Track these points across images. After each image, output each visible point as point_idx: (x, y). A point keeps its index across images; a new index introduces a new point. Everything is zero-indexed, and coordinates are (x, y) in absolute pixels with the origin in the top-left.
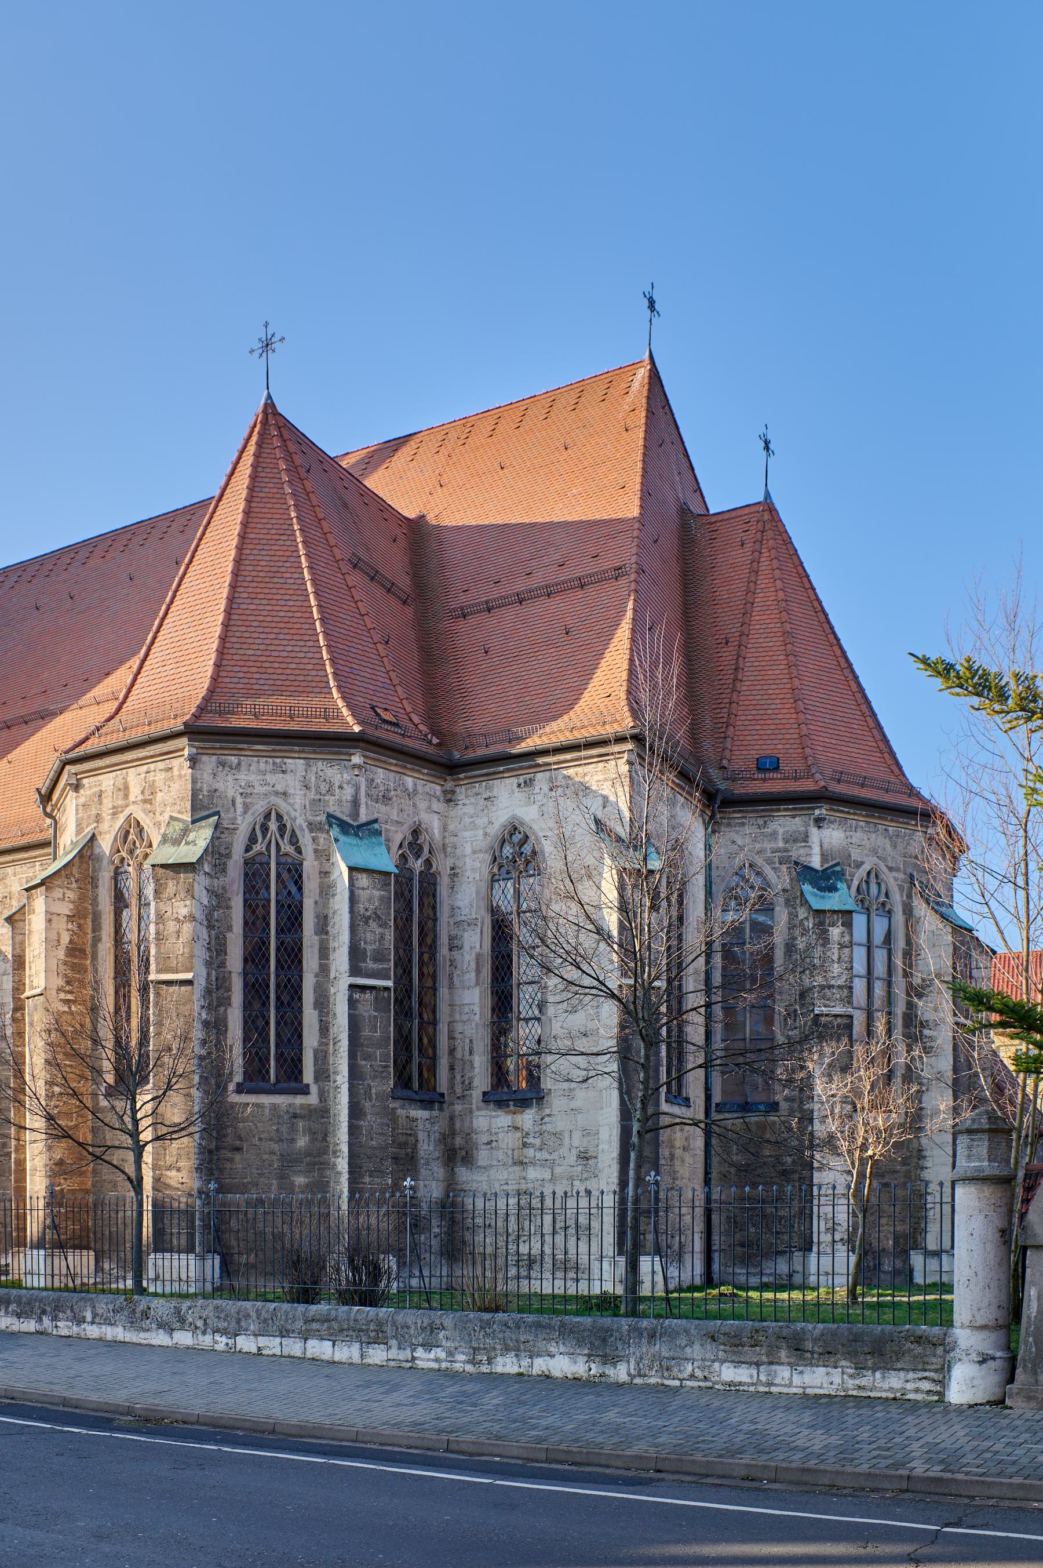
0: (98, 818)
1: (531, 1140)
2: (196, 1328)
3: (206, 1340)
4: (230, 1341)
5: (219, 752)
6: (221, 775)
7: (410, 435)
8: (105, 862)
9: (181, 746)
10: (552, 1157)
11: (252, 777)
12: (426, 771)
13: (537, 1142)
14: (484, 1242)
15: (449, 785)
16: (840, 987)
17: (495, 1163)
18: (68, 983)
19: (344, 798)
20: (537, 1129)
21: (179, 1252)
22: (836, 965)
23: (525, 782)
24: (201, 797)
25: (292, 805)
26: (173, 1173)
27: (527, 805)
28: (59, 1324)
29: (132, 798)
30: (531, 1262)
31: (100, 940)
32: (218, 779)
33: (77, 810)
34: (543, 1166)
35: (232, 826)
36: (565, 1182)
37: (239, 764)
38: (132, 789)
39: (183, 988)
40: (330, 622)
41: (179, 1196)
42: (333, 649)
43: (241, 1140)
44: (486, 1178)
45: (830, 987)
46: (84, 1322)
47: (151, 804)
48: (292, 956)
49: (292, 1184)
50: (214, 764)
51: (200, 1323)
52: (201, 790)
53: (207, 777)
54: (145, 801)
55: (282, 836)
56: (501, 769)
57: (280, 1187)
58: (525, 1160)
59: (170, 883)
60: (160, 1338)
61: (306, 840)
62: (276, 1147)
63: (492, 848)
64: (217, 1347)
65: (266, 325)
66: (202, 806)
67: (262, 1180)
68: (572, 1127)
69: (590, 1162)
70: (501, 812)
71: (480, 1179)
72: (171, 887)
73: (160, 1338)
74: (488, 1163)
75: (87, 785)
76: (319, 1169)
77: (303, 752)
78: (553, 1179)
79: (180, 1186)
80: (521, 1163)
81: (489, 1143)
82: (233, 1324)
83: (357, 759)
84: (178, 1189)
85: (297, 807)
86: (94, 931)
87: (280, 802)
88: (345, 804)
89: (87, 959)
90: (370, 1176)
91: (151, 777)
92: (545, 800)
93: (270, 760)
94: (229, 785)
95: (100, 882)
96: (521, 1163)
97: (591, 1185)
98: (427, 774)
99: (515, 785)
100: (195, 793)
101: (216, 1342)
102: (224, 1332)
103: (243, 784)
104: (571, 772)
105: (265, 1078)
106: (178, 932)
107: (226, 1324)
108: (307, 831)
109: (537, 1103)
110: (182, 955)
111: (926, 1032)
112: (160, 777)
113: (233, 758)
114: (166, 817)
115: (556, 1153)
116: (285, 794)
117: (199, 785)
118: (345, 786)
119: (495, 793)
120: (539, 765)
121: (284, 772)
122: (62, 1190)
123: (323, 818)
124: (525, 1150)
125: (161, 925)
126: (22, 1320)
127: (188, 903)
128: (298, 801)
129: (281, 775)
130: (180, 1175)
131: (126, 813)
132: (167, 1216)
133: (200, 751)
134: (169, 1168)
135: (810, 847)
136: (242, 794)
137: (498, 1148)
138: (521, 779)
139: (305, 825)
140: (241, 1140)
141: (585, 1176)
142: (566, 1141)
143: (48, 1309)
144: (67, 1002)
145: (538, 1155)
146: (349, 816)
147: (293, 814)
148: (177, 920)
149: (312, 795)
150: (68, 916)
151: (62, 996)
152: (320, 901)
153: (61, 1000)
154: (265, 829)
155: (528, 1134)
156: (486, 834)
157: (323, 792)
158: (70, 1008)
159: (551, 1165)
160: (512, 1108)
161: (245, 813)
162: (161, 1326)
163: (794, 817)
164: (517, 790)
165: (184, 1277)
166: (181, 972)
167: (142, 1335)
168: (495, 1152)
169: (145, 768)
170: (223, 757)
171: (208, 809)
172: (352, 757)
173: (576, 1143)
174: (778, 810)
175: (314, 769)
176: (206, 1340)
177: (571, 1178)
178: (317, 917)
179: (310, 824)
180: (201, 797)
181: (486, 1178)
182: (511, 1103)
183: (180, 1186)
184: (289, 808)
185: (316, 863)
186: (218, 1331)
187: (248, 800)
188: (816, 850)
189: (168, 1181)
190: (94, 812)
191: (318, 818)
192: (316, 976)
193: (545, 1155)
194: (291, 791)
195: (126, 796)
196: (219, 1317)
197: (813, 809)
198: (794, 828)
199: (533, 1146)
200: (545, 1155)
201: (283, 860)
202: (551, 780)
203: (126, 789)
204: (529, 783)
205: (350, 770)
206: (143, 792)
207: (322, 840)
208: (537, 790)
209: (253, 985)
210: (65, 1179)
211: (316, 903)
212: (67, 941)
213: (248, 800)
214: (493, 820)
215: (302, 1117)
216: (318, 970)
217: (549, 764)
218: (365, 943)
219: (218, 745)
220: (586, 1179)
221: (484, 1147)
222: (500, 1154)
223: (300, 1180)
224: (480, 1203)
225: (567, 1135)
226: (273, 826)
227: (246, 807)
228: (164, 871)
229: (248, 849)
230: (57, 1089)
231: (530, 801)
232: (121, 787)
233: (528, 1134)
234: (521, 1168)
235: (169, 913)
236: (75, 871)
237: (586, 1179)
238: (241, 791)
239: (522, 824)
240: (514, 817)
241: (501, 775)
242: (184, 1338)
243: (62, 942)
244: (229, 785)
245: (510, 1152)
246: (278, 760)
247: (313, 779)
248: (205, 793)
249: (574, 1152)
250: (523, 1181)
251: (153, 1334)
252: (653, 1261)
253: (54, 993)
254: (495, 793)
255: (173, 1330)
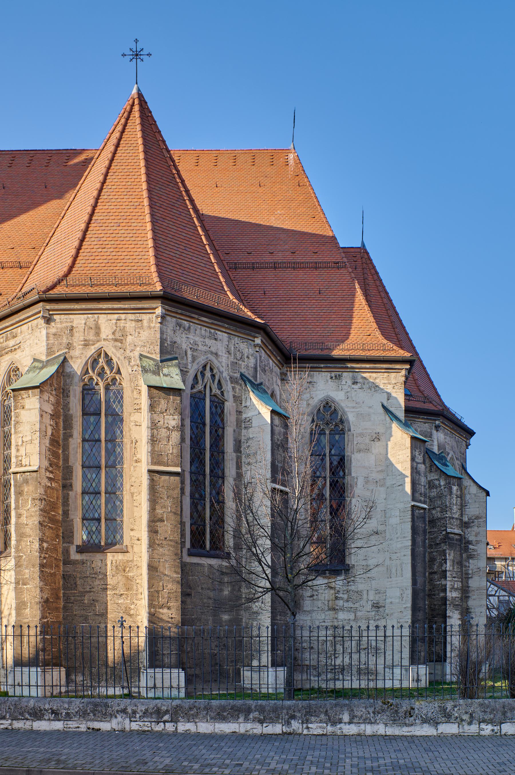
0: (69, 346)
1: (341, 595)
2: (462, 720)
3: (473, 729)
4: (495, 728)
5: (178, 316)
6: (178, 333)
7: (84, 150)
8: (76, 380)
9: (154, 306)
10: (355, 606)
11: (197, 339)
12: (279, 358)
13: (345, 596)
14: (309, 658)
15: (284, 370)
16: (456, 519)
17: (316, 609)
18: (51, 465)
19: (250, 365)
20: (345, 589)
21: (170, 667)
22: (455, 507)
23: (336, 376)
24: (166, 345)
25: (221, 363)
26: (165, 611)
27: (337, 390)
28: (310, 725)
29: (103, 336)
30: (343, 670)
31: (71, 436)
32: (177, 335)
33: (48, 337)
34: (349, 611)
35: (185, 369)
36: (364, 621)
37: (189, 328)
38: (103, 329)
39: (172, 478)
40: (160, 250)
41: (170, 628)
42: (160, 267)
43: (191, 588)
44: (310, 618)
45: (453, 518)
46: (340, 723)
47: (121, 343)
48: (218, 463)
49: (221, 619)
50: (174, 324)
51: (466, 717)
52: (166, 340)
53: (170, 332)
54: (116, 340)
55: (213, 381)
56: (322, 365)
57: (214, 621)
58: (337, 608)
59: (163, 401)
60: (427, 730)
61: (228, 387)
62: (211, 594)
63: (312, 413)
64: (482, 733)
65: (136, 41)
66: (168, 353)
67: (203, 616)
68: (368, 588)
69: (381, 609)
70: (318, 392)
71: (305, 618)
72: (163, 404)
73: (427, 730)
74: (311, 609)
75: (58, 320)
76: (236, 610)
77: (229, 329)
78: (356, 619)
79: (170, 620)
80: (334, 609)
81: (312, 596)
82: (499, 715)
83: (258, 341)
84: (168, 622)
85: (224, 364)
86: (65, 429)
87: (212, 358)
88: (250, 369)
89: (60, 449)
90: (280, 615)
91: (122, 324)
92: (349, 389)
93: (208, 329)
94: (183, 340)
95: (71, 394)
96: (334, 609)
97: (381, 623)
98: (279, 361)
99: (329, 377)
100: (163, 341)
101: (483, 730)
102: (490, 722)
103: (192, 342)
104: (365, 375)
105: (203, 546)
106: (168, 437)
107: (492, 716)
108: (229, 382)
109: (345, 573)
110: (172, 454)
111: (471, 547)
112: (130, 326)
113: (186, 322)
114: (137, 354)
115: (358, 604)
116: (216, 354)
117: (165, 336)
118: (250, 357)
119: (315, 379)
120: (347, 368)
121: (216, 339)
122: (48, 621)
123: (238, 375)
124: (337, 602)
125: (155, 431)
126: (265, 725)
127: (176, 417)
128: (224, 360)
129: (214, 341)
130: (170, 612)
131: (98, 345)
132: (160, 641)
133: (167, 313)
134: (162, 607)
135: (433, 441)
136: (191, 348)
137: (318, 600)
138: (333, 374)
139: (228, 378)
140: (191, 588)
141: (377, 618)
142: (365, 596)
143: (298, 715)
144: (50, 479)
145: (346, 605)
146: (253, 377)
147: (222, 369)
148: (168, 428)
149: (232, 358)
150: (51, 415)
151: (48, 474)
152: (237, 430)
153: (47, 477)
154: (203, 375)
155: (338, 591)
156: (308, 405)
157: (238, 358)
158: (51, 484)
159: (355, 611)
160: (328, 575)
161: (193, 362)
162: (425, 721)
163: (425, 423)
164: (330, 380)
165: (175, 685)
166: (171, 466)
167: (405, 729)
168: (316, 602)
169: (116, 316)
170: (180, 321)
171: (171, 354)
172: (256, 339)
173: (371, 597)
174: (419, 418)
175: (233, 341)
176: (473, 729)
177: (368, 619)
178: (235, 440)
179: (231, 378)
180: (166, 345)
181: (310, 618)
182: (327, 572)
183: (170, 620)
184: (219, 364)
185: (234, 404)
186: (484, 721)
187: (195, 354)
188: (436, 443)
189: (161, 616)
190: (65, 341)
191: (236, 375)
192: (235, 480)
193: (350, 604)
194: (220, 353)
195: (98, 333)
196: (485, 712)
197: (435, 420)
198: (425, 429)
199: (342, 599)
200: (350, 604)
201: (214, 398)
202: (354, 378)
203: (97, 329)
204: (338, 377)
205: (253, 347)
206: (114, 333)
207: (237, 390)
208: (344, 382)
209: (195, 481)
210: (49, 613)
211: (234, 431)
212: (50, 434)
213: (195, 354)
214: (314, 396)
215: (227, 574)
216: (235, 477)
217: (321, 368)
218: (278, 462)
219: (180, 311)
220: (378, 620)
221: (309, 599)
222: (319, 604)
223: (226, 617)
224: (306, 633)
225: (365, 593)
226: (208, 374)
227: (194, 358)
228: (157, 392)
229: (193, 387)
230: (45, 545)
231: (339, 389)
232: (93, 327)
233: (338, 591)
234: (334, 612)
235: (161, 423)
236: (55, 381)
237: (378, 620)
238: (191, 346)
239: (334, 402)
240: (328, 396)
241: (320, 370)
242: (450, 729)
243: (48, 434)
244: (183, 340)
245: (326, 603)
246: (213, 331)
247: (233, 348)
248: (169, 343)
249: (370, 603)
250: (335, 620)
251: (418, 728)
252: (426, 668)
253: (43, 471)
254: (315, 379)
255: (438, 723)
